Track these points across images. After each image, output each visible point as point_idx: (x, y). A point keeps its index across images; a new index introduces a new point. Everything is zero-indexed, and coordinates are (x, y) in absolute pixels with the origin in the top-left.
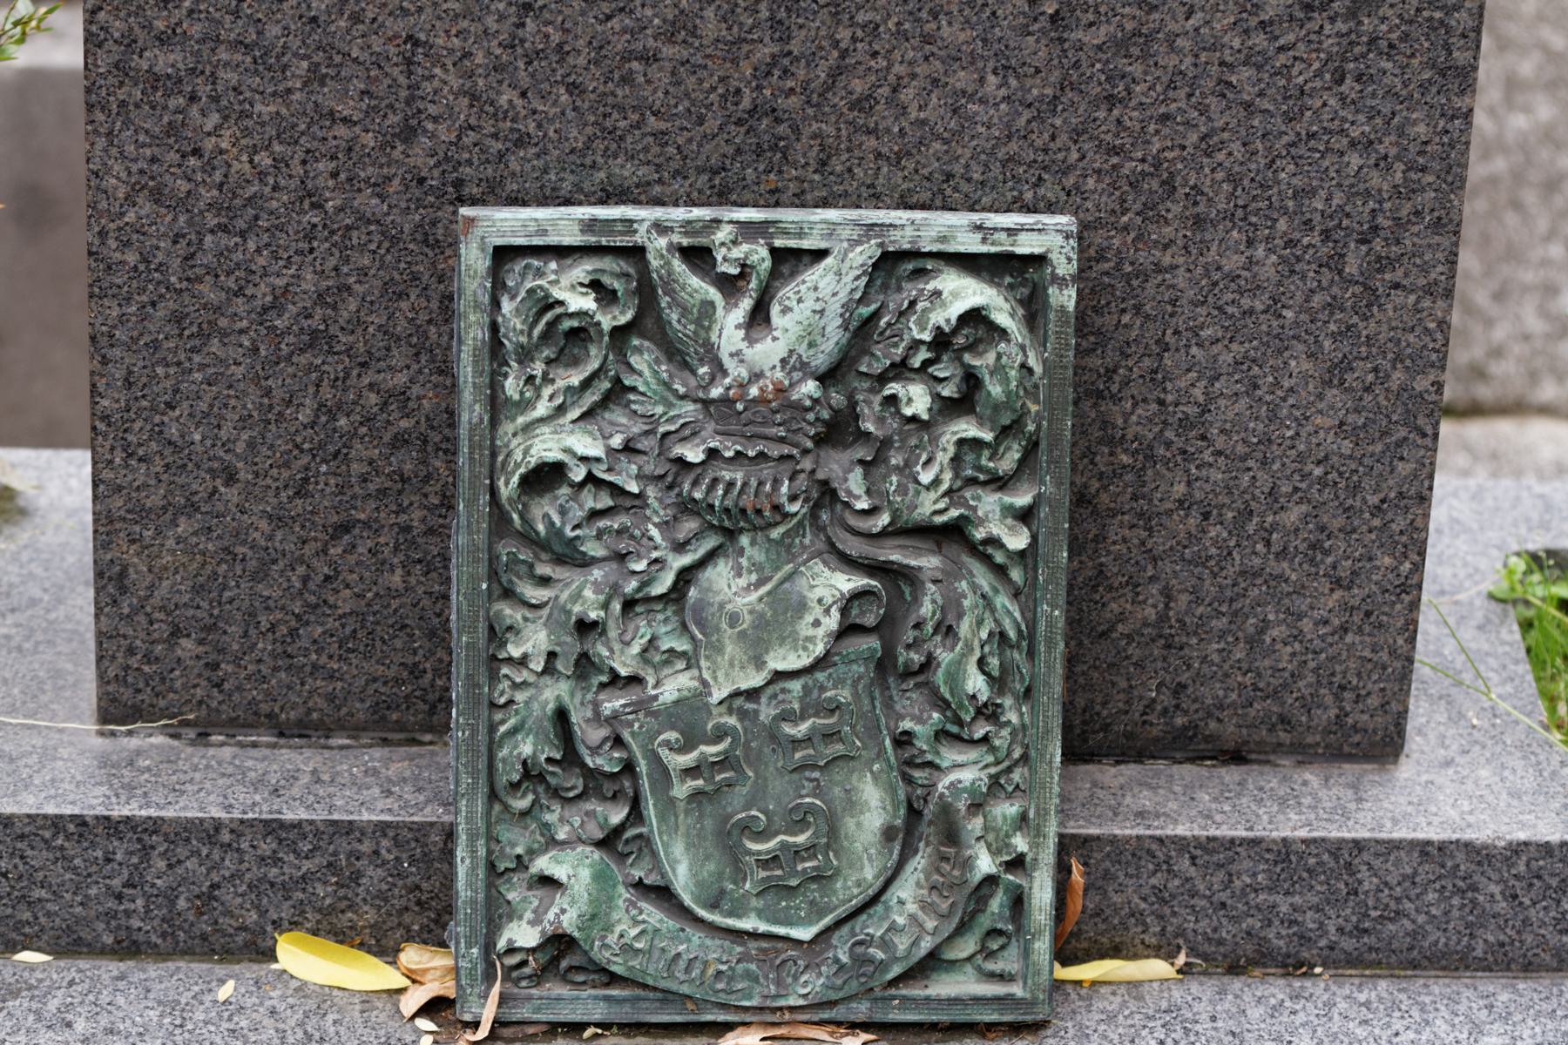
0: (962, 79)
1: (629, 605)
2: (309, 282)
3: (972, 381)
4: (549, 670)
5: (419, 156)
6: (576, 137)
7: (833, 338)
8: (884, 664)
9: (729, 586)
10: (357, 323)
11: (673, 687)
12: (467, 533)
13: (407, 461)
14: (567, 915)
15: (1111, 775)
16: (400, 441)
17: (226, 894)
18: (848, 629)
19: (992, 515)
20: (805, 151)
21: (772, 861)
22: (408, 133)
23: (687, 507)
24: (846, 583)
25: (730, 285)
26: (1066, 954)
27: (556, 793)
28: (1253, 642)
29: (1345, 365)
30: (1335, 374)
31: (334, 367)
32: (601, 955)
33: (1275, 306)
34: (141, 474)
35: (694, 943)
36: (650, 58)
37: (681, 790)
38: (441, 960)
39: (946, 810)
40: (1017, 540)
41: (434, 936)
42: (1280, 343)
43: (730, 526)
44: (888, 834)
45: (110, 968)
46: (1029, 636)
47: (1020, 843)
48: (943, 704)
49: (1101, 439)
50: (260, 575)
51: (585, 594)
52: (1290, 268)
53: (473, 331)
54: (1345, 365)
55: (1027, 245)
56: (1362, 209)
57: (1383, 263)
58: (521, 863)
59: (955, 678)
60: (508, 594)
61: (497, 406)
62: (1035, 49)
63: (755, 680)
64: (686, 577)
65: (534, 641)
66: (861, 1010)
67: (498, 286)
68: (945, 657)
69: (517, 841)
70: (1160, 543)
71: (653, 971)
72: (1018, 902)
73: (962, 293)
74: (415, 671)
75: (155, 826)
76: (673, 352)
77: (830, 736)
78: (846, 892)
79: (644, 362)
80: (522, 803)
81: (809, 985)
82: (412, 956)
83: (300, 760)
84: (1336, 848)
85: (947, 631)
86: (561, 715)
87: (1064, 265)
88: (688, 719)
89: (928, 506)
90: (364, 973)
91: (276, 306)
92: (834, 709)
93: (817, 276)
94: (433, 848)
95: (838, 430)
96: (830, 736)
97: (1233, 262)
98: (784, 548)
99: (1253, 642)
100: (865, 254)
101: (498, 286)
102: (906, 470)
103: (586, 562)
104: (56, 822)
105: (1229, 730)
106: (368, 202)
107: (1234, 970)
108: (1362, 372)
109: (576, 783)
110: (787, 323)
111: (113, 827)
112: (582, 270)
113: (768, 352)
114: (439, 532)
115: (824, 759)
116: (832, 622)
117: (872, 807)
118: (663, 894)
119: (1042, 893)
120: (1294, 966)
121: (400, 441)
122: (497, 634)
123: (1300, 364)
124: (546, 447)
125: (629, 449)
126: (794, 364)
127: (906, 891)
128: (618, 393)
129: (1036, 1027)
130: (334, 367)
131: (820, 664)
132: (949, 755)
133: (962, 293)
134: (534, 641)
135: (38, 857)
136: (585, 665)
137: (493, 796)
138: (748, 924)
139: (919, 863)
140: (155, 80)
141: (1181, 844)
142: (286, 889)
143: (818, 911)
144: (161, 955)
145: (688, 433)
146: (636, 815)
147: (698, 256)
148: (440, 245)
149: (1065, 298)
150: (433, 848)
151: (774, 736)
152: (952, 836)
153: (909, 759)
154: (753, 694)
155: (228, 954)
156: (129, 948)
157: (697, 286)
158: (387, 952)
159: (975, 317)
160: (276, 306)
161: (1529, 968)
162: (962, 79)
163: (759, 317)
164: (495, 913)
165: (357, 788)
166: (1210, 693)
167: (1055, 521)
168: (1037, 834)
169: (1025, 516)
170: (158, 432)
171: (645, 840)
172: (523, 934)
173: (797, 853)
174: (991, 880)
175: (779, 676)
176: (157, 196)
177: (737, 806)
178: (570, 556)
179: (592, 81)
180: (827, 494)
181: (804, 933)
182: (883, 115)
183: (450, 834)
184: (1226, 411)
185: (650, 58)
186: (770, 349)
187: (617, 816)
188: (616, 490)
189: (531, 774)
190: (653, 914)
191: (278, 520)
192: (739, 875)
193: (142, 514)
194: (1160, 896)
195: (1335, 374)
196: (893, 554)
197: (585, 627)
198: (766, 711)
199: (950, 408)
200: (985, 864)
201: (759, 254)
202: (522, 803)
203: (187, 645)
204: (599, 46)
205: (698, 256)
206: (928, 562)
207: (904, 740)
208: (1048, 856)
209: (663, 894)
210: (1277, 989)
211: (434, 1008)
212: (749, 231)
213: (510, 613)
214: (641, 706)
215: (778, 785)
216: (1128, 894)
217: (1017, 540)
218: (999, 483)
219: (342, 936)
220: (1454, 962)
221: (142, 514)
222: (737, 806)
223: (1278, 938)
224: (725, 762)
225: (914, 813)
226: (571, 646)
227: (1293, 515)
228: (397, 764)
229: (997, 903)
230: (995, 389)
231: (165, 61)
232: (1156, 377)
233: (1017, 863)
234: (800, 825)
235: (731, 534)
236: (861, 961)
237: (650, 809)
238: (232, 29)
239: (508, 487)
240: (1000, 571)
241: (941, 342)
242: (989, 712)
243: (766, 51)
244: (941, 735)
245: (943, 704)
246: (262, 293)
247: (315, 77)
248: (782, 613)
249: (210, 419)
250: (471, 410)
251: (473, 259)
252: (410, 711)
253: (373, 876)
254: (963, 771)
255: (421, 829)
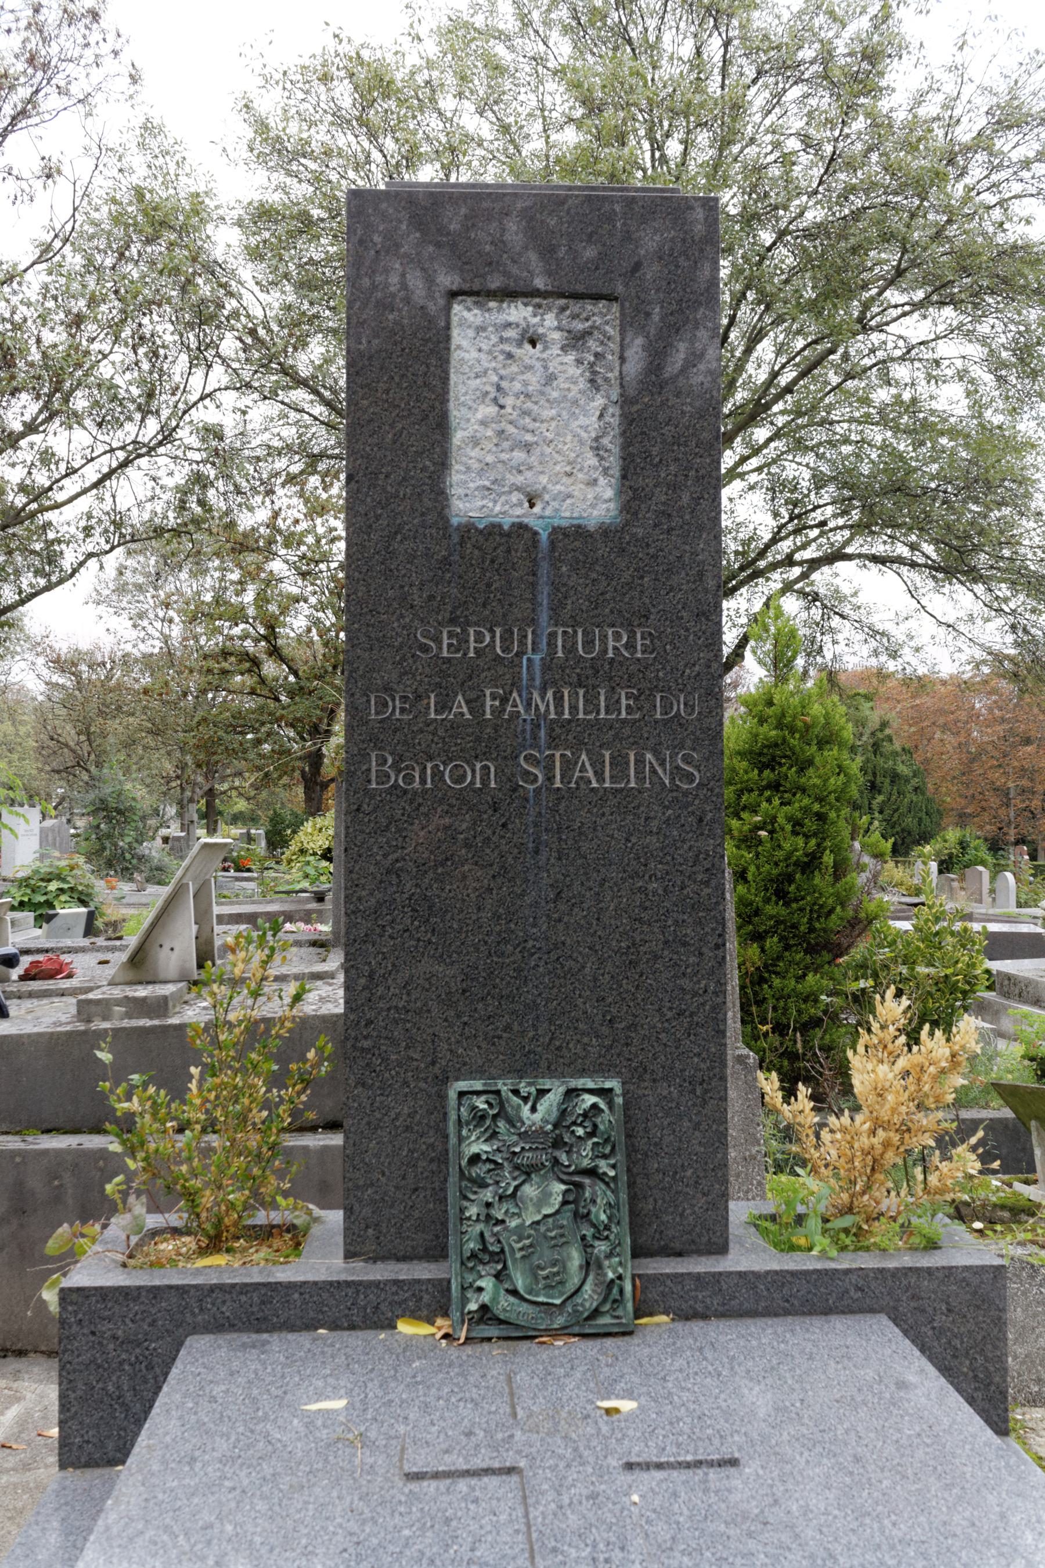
0: (586, 1040)
1: (501, 1198)
2: (406, 1111)
3: (595, 1126)
4: (478, 1220)
5: (436, 1070)
6: (480, 1062)
7: (555, 1114)
8: (576, 1214)
9: (529, 1191)
10: (419, 1123)
11: (513, 1223)
12: (453, 1179)
13: (434, 1166)
14: (485, 1298)
15: (644, 1261)
16: (432, 1160)
17: (383, 1307)
18: (565, 1203)
19: (603, 1166)
20: (544, 1064)
21: (546, 1278)
22: (433, 1063)
23: (517, 1167)
24: (563, 1187)
25: (525, 1099)
26: (637, 1317)
27: (481, 1262)
28: (681, 1215)
29: (699, 1124)
30: (697, 1126)
31: (413, 1137)
32: (496, 1312)
33: (678, 1106)
34: (358, 1174)
35: (524, 1307)
36: (500, 1037)
37: (518, 1255)
38: (448, 1323)
39: (598, 1258)
40: (612, 1173)
41: (446, 1315)
42: (680, 1117)
43: (527, 1172)
44: (581, 1267)
45: (346, 1333)
46: (618, 1204)
47: (620, 1270)
48: (594, 1226)
49: (633, 1143)
50: (392, 1206)
51: (488, 1195)
52: (681, 1093)
53: (453, 1117)
54: (699, 1124)
55: (608, 1085)
56: (699, 1074)
57: (706, 1091)
58: (471, 1286)
59: (597, 1216)
60: (466, 1198)
61: (461, 1139)
62: (605, 1030)
63: (538, 1218)
64: (517, 1188)
65: (473, 1211)
66: (576, 1330)
67: (460, 1104)
68: (594, 1210)
69: (470, 1278)
70: (652, 1183)
71: (513, 1318)
72: (621, 1291)
73: (590, 1100)
74: (437, 1237)
75: (360, 1283)
76: (511, 1122)
77: (562, 1236)
78: (570, 1287)
79: (502, 1124)
80: (471, 1265)
81: (560, 1321)
82: (439, 1322)
83: (404, 1266)
84: (714, 1275)
85: (594, 1201)
86: (482, 1234)
87: (618, 1090)
88: (519, 1232)
89: (586, 1163)
90: (425, 1329)
91: (396, 1119)
92: (562, 1227)
93: (550, 1095)
94: (443, 1286)
95: (558, 1143)
96: (562, 1236)
97: (665, 1093)
98: (544, 1177)
99: (681, 1215)
100: (562, 1089)
101: (460, 1104)
102: (578, 1152)
103: (487, 1186)
104: (331, 1283)
105: (677, 1245)
106: (422, 1085)
107: (687, 1319)
108: (704, 1126)
109: (487, 1258)
110: (542, 1107)
111: (348, 1284)
112: (483, 1098)
113: (537, 1117)
114: (443, 1189)
115: (560, 1244)
116: (560, 1198)
117: (575, 1259)
118: (514, 1293)
119: (628, 1287)
120: (705, 1317)
121: (432, 1160)
122: (462, 1211)
123: (686, 1124)
124: (475, 1149)
125: (498, 1150)
126: (545, 1121)
127: (588, 1287)
128: (494, 1135)
129: (630, 1333)
130: (413, 1137)
131: (557, 1212)
132: (597, 1243)
133: (590, 1100)
134: (473, 1211)
135: (325, 1295)
136: (488, 1217)
137: (462, 1263)
138: (541, 1299)
139: (591, 1277)
140: (363, 1049)
141: (668, 1275)
142: (400, 1304)
143: (561, 1294)
144: (361, 1328)
145: (515, 1144)
146: (505, 1267)
147: (516, 1092)
148: (443, 1097)
149: (619, 1100)
150: (443, 1286)
151: (545, 1237)
152: (600, 1266)
153: (586, 1245)
154: (538, 1223)
155: (383, 1328)
156: (352, 1327)
157: (515, 1099)
158: (432, 1323)
159: (594, 1106)
160: (396, 1119)
161: (776, 1315)
162: (586, 1040)
163: (534, 1109)
164: (465, 1301)
165: (423, 1271)
166: (670, 1233)
167: (622, 1168)
168: (625, 1268)
169: (614, 1167)
170: (363, 1161)
171: (509, 1276)
172: (473, 1306)
173: (555, 1274)
174: (612, 1281)
175: (546, 1216)
176: (363, 1085)
177: (536, 1261)
178: (484, 1185)
179: (484, 1045)
180: (556, 1162)
181: (558, 1302)
182: (564, 1051)
183: (449, 1282)
184: (667, 1139)
185: (500, 1037)
186: (538, 1116)
187: (500, 1267)
188: (495, 1162)
189: (473, 1256)
190: (512, 1299)
191: (397, 1188)
192: (537, 1282)
193: (357, 1187)
194: (663, 1294)
195: (697, 1126)
196: (577, 1179)
197: (488, 1205)
198: (543, 1229)
199: (591, 1135)
200: (611, 1275)
201: (533, 1090)
202: (471, 1265)
203: (370, 1231)
204: (486, 1034)
205: (516, 1092)
206: (587, 1181)
207: (583, 1238)
208: (629, 1276)
209: (514, 1293)
210: (701, 1323)
211: (446, 1336)
212: (529, 1084)
213: (465, 1203)
214: (506, 1229)
215: (547, 1253)
216: (653, 1294)
217: (612, 1173)
218: (605, 1157)
219: (419, 1318)
220: (752, 1314)
221: (357, 1187)
222: (536, 1261)
223: (699, 1307)
224: (531, 1246)
225: (588, 1264)
226: (484, 1211)
227: (689, 1173)
228: (433, 1266)
229: (615, 1291)
230: (602, 1127)
231: (366, 1044)
232: (646, 1130)
233: (620, 1277)
234: (554, 1265)
235: (528, 1174)
236: (576, 1311)
237: (509, 1263)
238: (384, 1033)
239: (464, 1162)
240: (607, 1184)
241: (585, 1115)
242: (607, 1227)
243: (531, 1034)
244: (594, 1237)
245: (594, 1226)
246: (393, 1115)
247: (407, 1047)
248: (545, 1198)
249: (377, 1156)
250: (453, 1140)
251: (452, 1095)
252: (437, 1252)
253: (426, 1298)
254: (601, 1247)
255: (440, 1280)
